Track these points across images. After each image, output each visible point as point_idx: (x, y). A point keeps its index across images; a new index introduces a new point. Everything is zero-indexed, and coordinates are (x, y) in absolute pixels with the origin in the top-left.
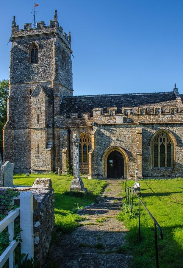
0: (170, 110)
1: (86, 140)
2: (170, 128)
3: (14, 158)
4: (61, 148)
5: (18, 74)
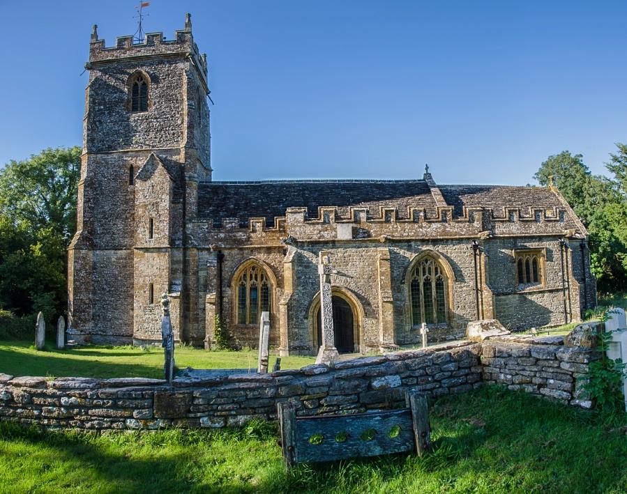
0: (440, 212)
1: (256, 275)
2: (440, 248)
3: (92, 311)
4: (201, 293)
5: (103, 134)
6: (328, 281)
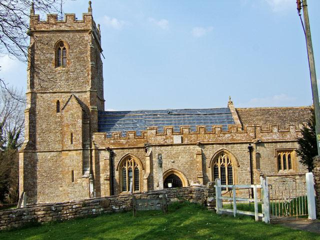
6: (161, 165)
